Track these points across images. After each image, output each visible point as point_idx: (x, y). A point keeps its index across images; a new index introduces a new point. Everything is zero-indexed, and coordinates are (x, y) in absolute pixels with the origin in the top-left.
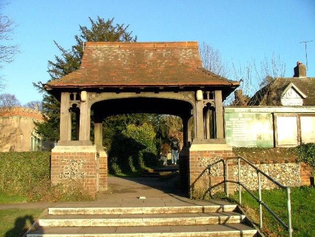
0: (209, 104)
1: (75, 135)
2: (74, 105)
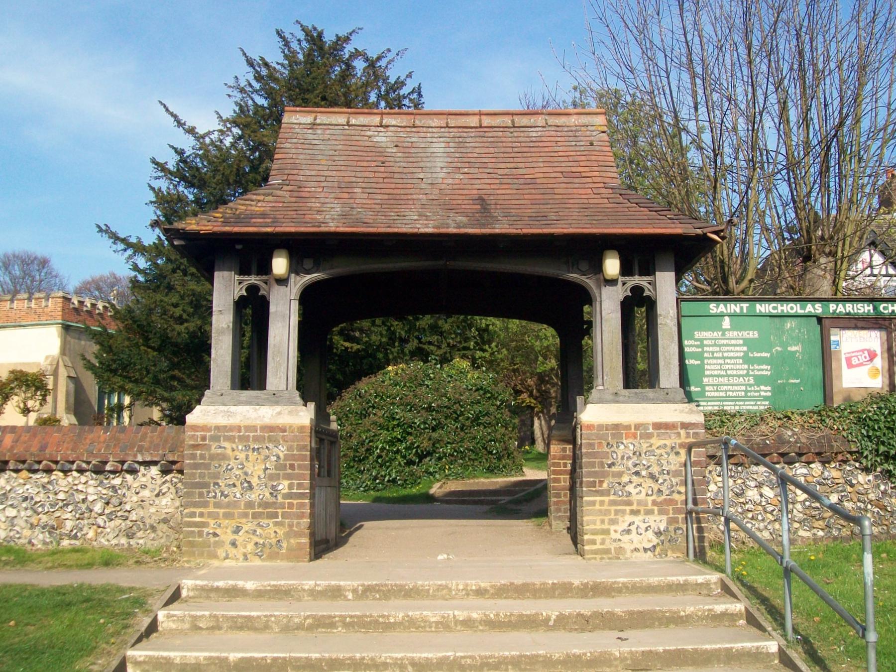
0: (637, 290)
1: (250, 374)
2: (253, 289)
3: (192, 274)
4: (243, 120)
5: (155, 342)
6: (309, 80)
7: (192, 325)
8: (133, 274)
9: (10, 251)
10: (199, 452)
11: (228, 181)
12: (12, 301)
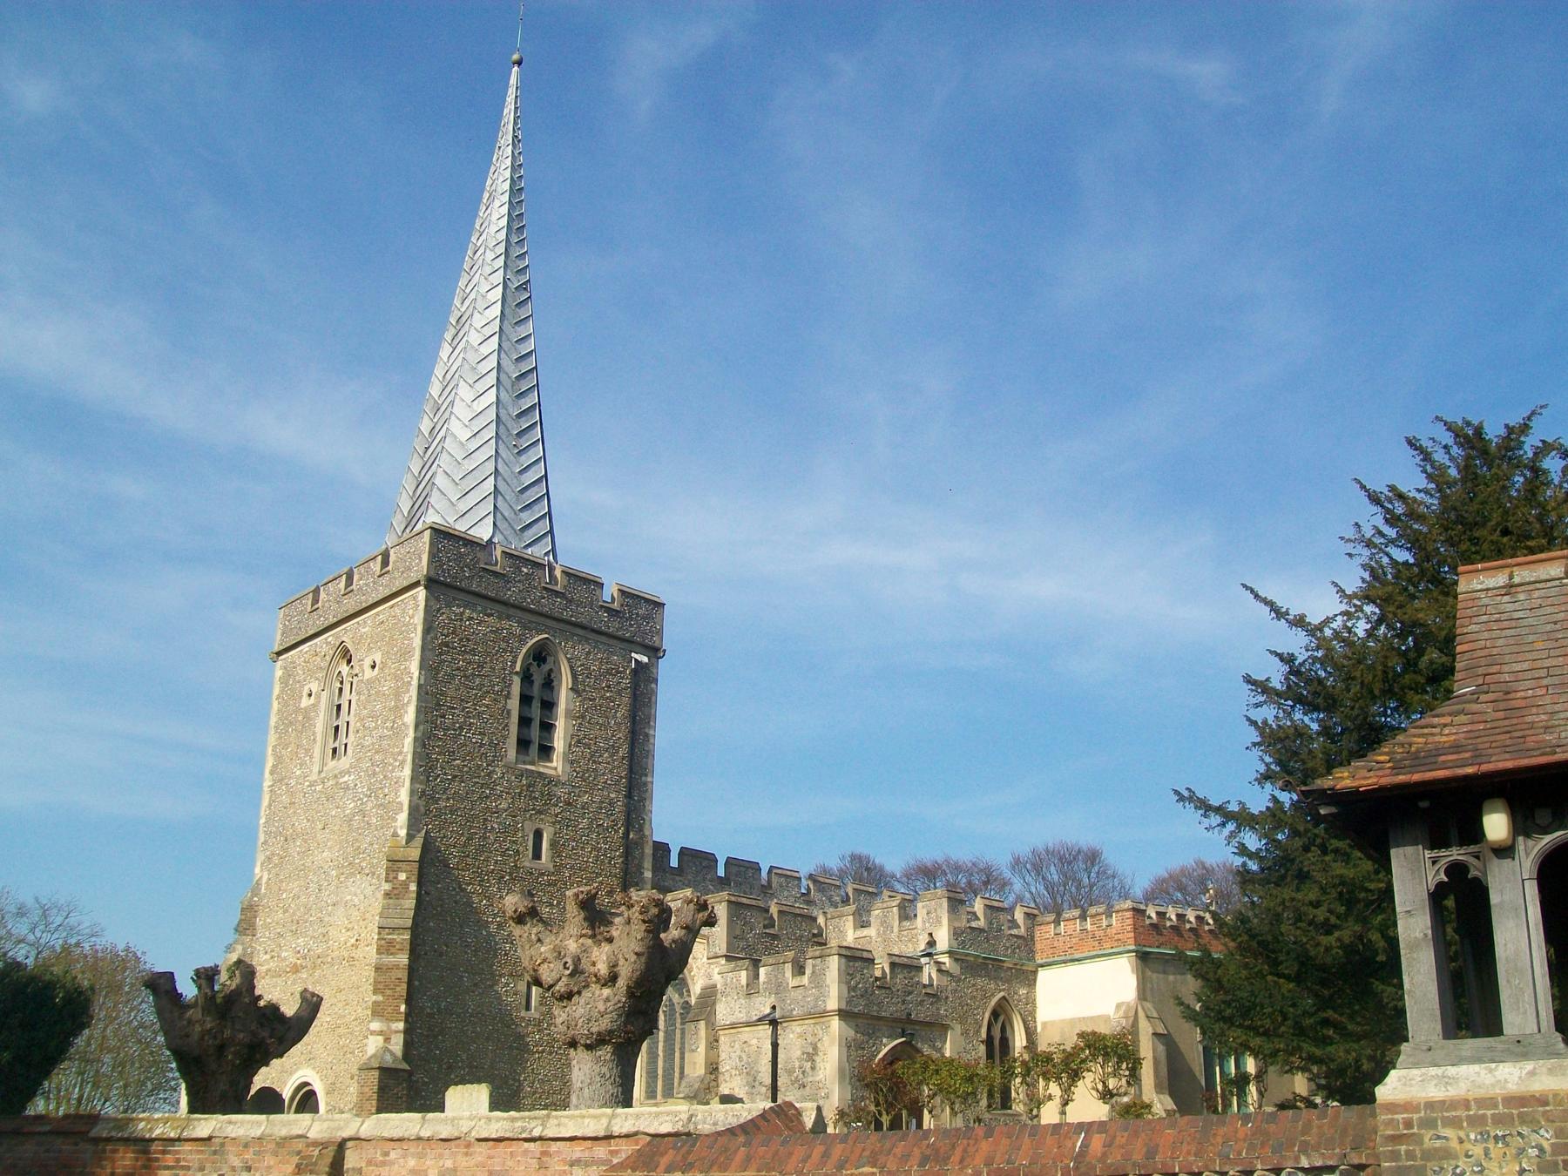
1: (1472, 1009)
2: (1456, 871)
3: (1336, 851)
4: (1381, 592)
5: (1289, 967)
6: (1475, 507)
7: (1346, 934)
8: (1238, 861)
9: (1041, 847)
10: (1403, 1148)
11: (1371, 692)
12: (1057, 922)
